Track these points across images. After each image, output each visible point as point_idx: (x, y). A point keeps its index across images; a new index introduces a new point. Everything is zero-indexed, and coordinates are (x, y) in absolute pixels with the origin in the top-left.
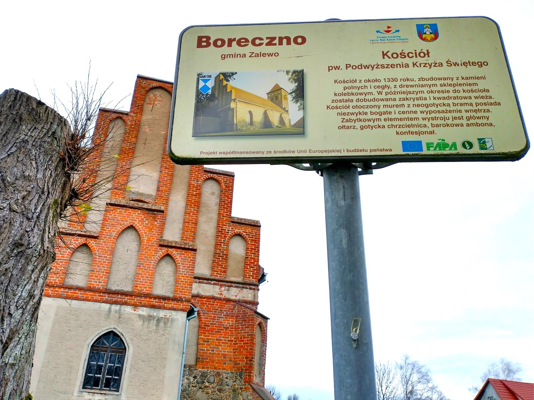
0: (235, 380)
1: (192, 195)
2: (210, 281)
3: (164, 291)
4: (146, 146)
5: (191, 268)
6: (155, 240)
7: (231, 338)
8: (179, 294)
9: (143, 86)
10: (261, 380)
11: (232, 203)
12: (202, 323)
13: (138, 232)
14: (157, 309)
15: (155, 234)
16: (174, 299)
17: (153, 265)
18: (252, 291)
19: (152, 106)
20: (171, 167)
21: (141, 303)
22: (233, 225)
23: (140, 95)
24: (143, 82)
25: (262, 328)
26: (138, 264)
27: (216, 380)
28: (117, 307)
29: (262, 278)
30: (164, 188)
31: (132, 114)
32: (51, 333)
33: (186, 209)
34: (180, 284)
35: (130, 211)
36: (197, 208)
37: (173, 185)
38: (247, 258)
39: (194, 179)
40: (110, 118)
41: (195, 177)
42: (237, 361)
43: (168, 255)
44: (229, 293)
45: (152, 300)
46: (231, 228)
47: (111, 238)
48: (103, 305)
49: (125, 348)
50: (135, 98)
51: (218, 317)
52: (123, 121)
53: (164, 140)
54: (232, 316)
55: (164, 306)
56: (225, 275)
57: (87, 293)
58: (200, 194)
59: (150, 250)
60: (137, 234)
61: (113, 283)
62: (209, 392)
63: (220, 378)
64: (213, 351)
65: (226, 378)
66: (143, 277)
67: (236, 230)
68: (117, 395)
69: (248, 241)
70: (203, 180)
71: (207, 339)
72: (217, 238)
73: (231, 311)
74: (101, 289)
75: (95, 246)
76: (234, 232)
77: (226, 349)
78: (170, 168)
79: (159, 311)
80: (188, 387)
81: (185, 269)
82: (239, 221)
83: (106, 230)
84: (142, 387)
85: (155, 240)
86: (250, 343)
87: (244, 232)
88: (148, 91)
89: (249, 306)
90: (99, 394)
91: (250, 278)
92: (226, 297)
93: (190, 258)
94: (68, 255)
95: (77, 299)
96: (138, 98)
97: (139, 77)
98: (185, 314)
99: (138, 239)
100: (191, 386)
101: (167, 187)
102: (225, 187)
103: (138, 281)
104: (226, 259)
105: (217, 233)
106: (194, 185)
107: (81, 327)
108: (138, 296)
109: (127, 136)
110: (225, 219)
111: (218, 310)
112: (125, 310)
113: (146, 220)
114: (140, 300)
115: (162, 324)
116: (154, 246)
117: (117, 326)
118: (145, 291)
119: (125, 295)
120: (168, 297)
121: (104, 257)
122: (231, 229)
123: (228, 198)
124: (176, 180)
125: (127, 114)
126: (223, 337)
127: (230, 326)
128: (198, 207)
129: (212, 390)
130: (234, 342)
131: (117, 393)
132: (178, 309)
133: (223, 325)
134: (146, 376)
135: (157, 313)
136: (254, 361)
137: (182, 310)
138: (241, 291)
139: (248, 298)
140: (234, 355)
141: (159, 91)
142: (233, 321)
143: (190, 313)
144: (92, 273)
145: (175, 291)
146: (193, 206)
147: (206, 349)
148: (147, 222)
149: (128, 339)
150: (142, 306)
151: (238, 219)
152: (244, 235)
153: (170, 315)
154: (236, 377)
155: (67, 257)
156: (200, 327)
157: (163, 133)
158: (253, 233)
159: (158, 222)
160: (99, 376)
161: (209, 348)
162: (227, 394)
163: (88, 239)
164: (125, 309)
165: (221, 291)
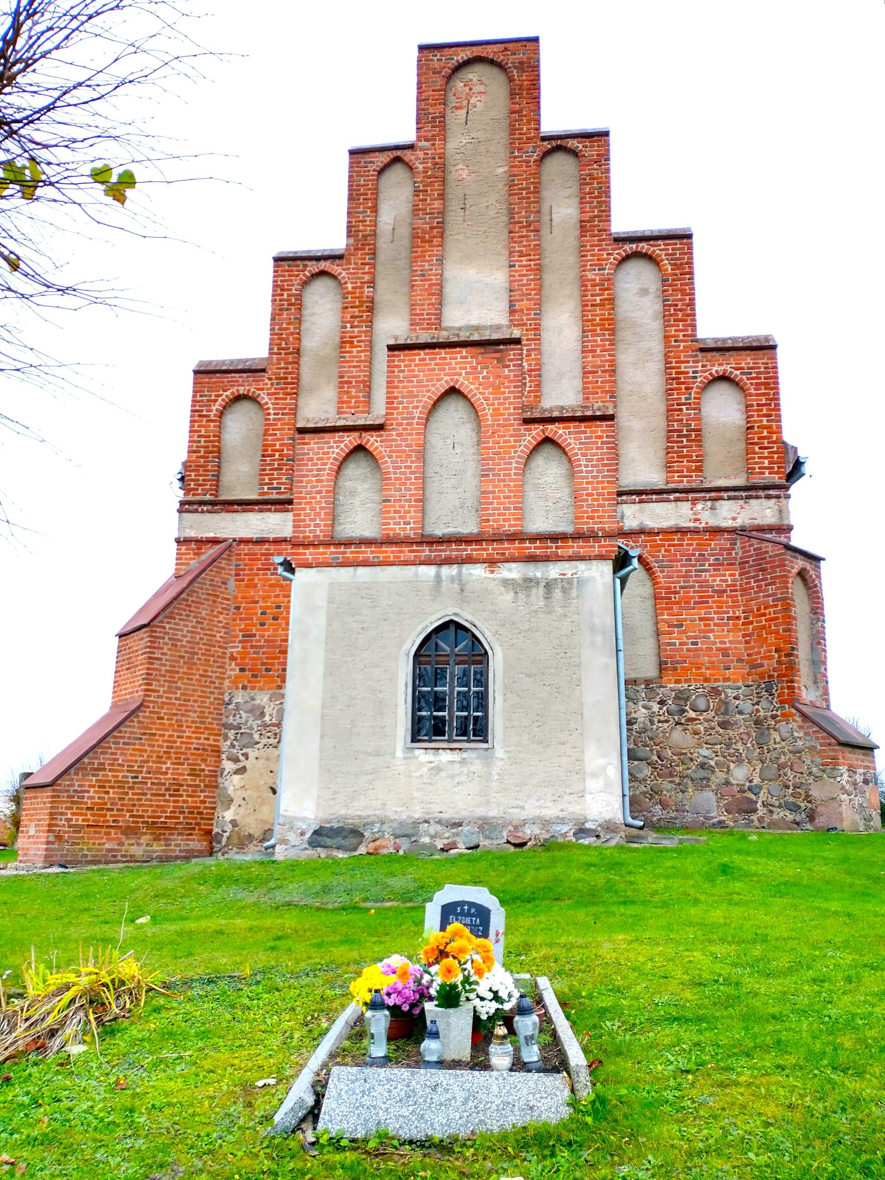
0: (756, 700)
1: (592, 305)
2: (665, 496)
3: (551, 522)
4: (467, 213)
5: (606, 462)
6: (512, 411)
7: (734, 612)
8: (588, 523)
9: (435, 69)
10: (821, 696)
11: (694, 304)
12: (660, 588)
13: (469, 400)
14: (541, 563)
15: (509, 398)
16: (578, 536)
17: (516, 468)
18: (773, 501)
19: (464, 111)
20: (531, 250)
21: (504, 554)
22: (703, 357)
23: (433, 91)
24: (435, 58)
25: (809, 582)
26: (483, 470)
27: (712, 705)
28: (453, 570)
29: (796, 471)
30: (525, 302)
31: (423, 144)
32: (327, 638)
33: (583, 342)
34: (587, 500)
35: (443, 355)
36: (609, 335)
37: (544, 292)
38: (752, 428)
39: (591, 265)
40: (371, 167)
41: (593, 260)
42: (756, 660)
43: (548, 440)
44: (715, 515)
45: (528, 545)
46: (700, 364)
47: (412, 424)
48: (423, 569)
49: (486, 653)
50: (423, 103)
51: (696, 571)
52: (405, 167)
53: (507, 188)
54: (732, 564)
55: (557, 555)
56: (699, 476)
57: (384, 549)
58: (613, 299)
59: (504, 436)
60: (467, 403)
61: (435, 520)
62: (699, 729)
63: (720, 700)
64: (696, 644)
65: (734, 698)
66: (499, 498)
67: (715, 369)
68: (486, 749)
69: (749, 389)
70: (613, 264)
71: (678, 620)
72: (670, 395)
73: (727, 554)
74: (412, 536)
75: (382, 446)
76: (711, 374)
77: (727, 636)
78: (532, 253)
79: (547, 567)
80: (649, 724)
81: (592, 466)
82: (720, 345)
83: (398, 408)
84: (536, 729)
85: (512, 411)
86: (783, 616)
87: (737, 369)
88: (449, 78)
89: (768, 536)
90: (448, 751)
91: (763, 473)
92: (710, 525)
93: (600, 437)
94: (328, 474)
95: (365, 564)
96: (430, 101)
97: (422, 48)
98: (607, 567)
99: (473, 416)
100: (656, 720)
101: (532, 299)
102: (672, 269)
103: (488, 509)
104: (699, 440)
105: (667, 384)
106: (595, 280)
107: (385, 620)
108: (494, 541)
109: (421, 200)
110: (682, 348)
111: (694, 555)
112: (471, 574)
113: (482, 368)
114: (500, 549)
115: (557, 594)
116: (512, 425)
117: (460, 608)
118: (508, 527)
119: (465, 541)
120: (564, 534)
121: (406, 467)
122: (700, 368)
123: (684, 293)
124: (549, 278)
125: (411, 147)
126: (715, 613)
127: (727, 586)
128: (613, 332)
129: (706, 724)
130: (743, 620)
131: (485, 746)
132: (590, 556)
133: (712, 587)
134: (541, 706)
135: (543, 572)
136: (797, 656)
137: (601, 557)
138: (745, 506)
139: (765, 520)
140: (746, 649)
141: (476, 70)
142: (734, 575)
143: (621, 561)
144: (386, 507)
145: (576, 518)
146: (598, 331)
147: (677, 642)
148: (485, 373)
149: (488, 634)
150: (507, 561)
151: (716, 340)
152: (736, 376)
153: (574, 571)
154: (757, 693)
155: (328, 481)
156: (656, 597)
157: (501, 170)
158: (759, 368)
159: (512, 368)
160: (441, 714)
161: (685, 640)
162: (741, 730)
163: (364, 434)
164: (472, 571)
165: (695, 514)
